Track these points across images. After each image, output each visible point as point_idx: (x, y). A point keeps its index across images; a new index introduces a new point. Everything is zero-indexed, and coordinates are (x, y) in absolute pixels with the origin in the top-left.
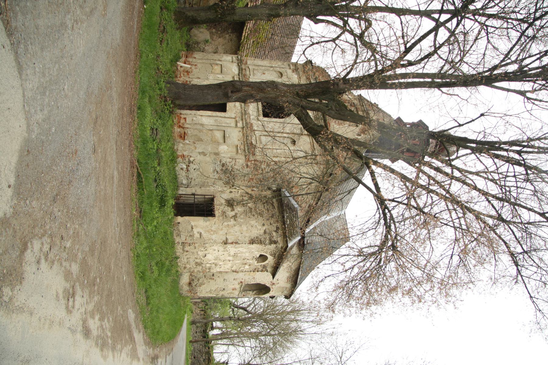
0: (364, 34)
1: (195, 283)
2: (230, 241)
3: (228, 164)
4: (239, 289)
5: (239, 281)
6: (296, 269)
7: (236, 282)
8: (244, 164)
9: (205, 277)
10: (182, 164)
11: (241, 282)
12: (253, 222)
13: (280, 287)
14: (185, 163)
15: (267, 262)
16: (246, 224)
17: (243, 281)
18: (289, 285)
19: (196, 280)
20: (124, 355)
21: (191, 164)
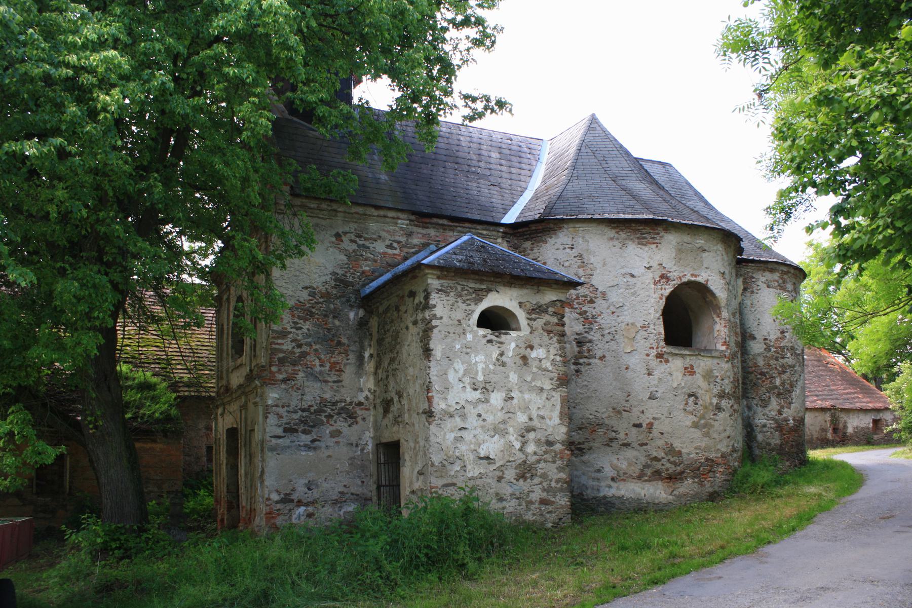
0: (53, 136)
1: (668, 465)
2: (426, 406)
3: (285, 420)
4: (688, 358)
5: (654, 363)
6: (614, 228)
7: (660, 370)
8: (283, 386)
9: (646, 444)
10: (294, 516)
11: (659, 356)
12: (405, 355)
13: (678, 259)
14: (290, 510)
15: (476, 316)
16: (407, 368)
17: (654, 352)
18: (671, 239)
19: (658, 466)
20: (156, 600)
21: (295, 497)
